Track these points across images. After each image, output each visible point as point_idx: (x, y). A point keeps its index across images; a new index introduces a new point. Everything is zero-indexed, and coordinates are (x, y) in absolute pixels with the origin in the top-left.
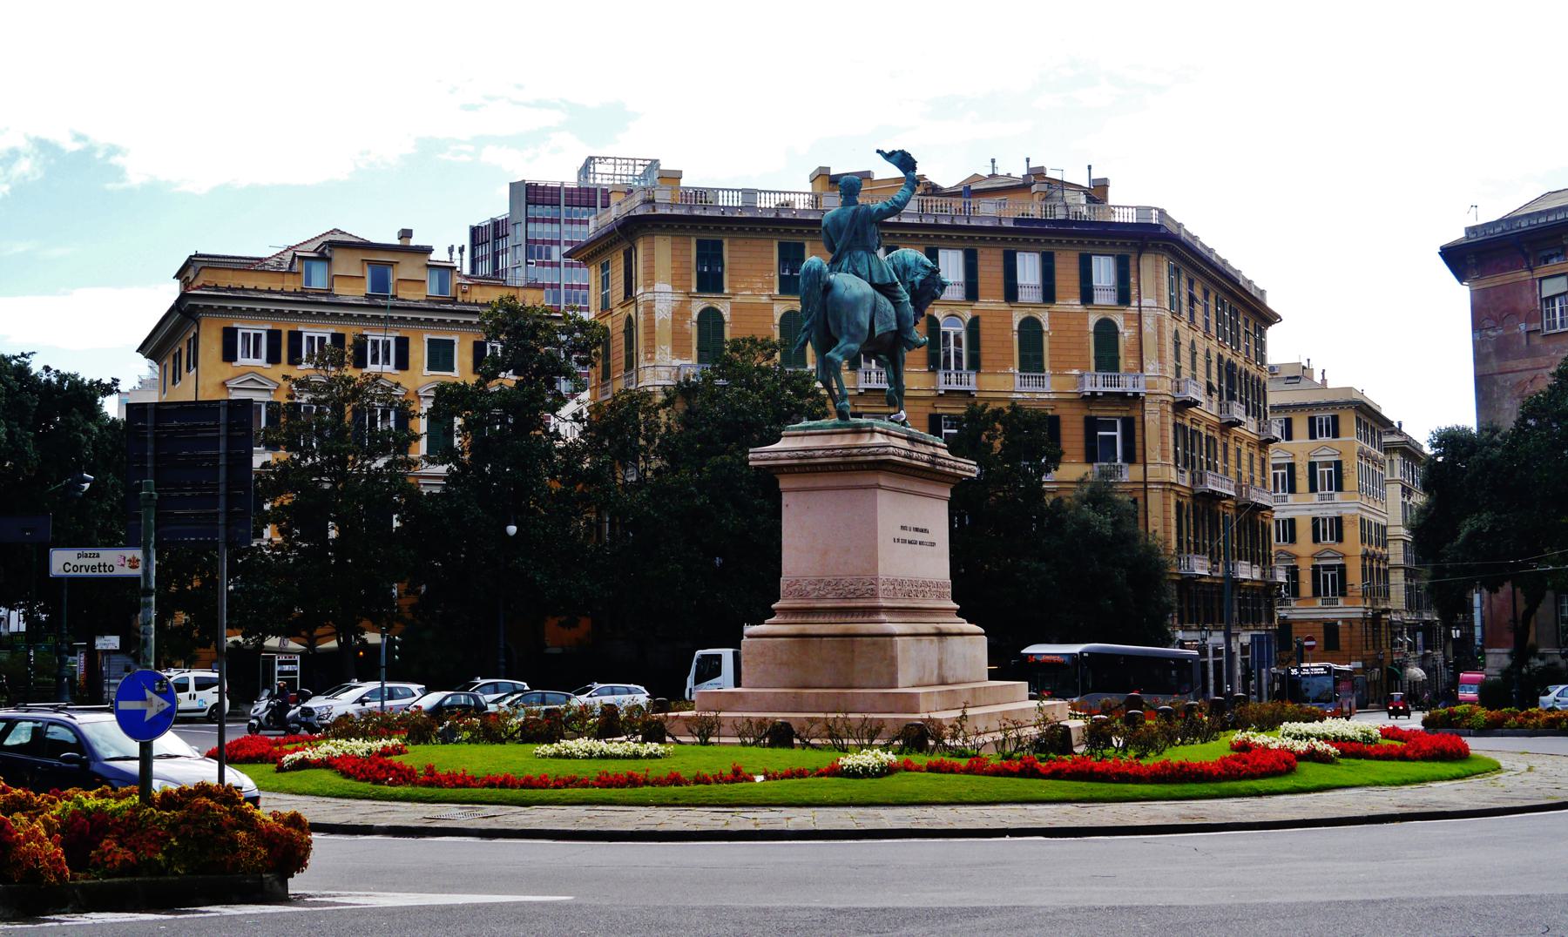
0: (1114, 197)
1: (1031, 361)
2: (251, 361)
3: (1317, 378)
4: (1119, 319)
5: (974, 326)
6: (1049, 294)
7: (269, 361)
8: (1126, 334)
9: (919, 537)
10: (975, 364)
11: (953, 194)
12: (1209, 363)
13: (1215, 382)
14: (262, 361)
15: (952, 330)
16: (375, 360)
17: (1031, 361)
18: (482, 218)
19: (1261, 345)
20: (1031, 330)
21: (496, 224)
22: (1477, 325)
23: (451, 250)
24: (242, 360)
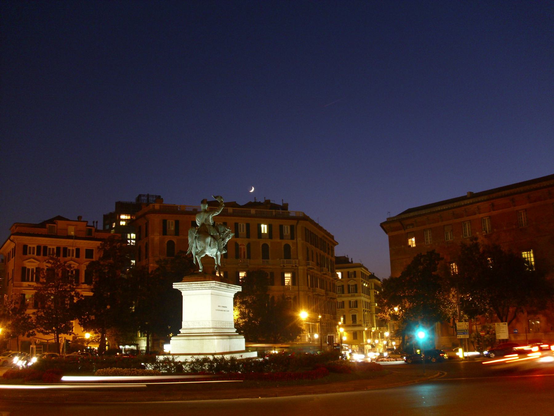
0: (290, 209)
1: (265, 256)
2: (32, 246)
3: (350, 261)
4: (291, 244)
5: (249, 246)
6: (293, 237)
7: (27, 246)
8: (293, 248)
9: (224, 309)
10: (249, 257)
11: (243, 207)
12: (317, 256)
13: (319, 262)
14: (29, 246)
15: (242, 247)
16: (30, 253)
17: (265, 256)
18: (107, 212)
19: (333, 250)
20: (265, 246)
21: (111, 213)
22: (390, 246)
23: (94, 222)
24: (35, 246)
